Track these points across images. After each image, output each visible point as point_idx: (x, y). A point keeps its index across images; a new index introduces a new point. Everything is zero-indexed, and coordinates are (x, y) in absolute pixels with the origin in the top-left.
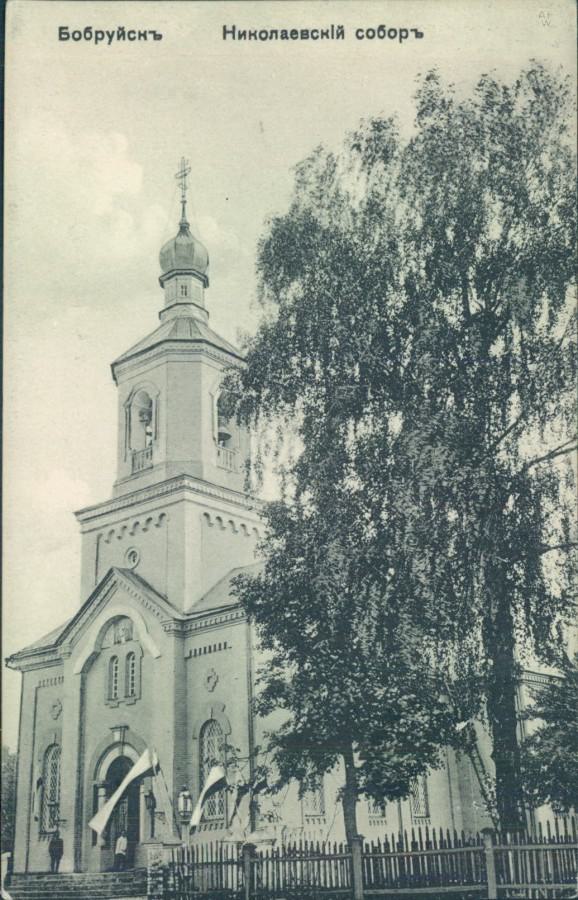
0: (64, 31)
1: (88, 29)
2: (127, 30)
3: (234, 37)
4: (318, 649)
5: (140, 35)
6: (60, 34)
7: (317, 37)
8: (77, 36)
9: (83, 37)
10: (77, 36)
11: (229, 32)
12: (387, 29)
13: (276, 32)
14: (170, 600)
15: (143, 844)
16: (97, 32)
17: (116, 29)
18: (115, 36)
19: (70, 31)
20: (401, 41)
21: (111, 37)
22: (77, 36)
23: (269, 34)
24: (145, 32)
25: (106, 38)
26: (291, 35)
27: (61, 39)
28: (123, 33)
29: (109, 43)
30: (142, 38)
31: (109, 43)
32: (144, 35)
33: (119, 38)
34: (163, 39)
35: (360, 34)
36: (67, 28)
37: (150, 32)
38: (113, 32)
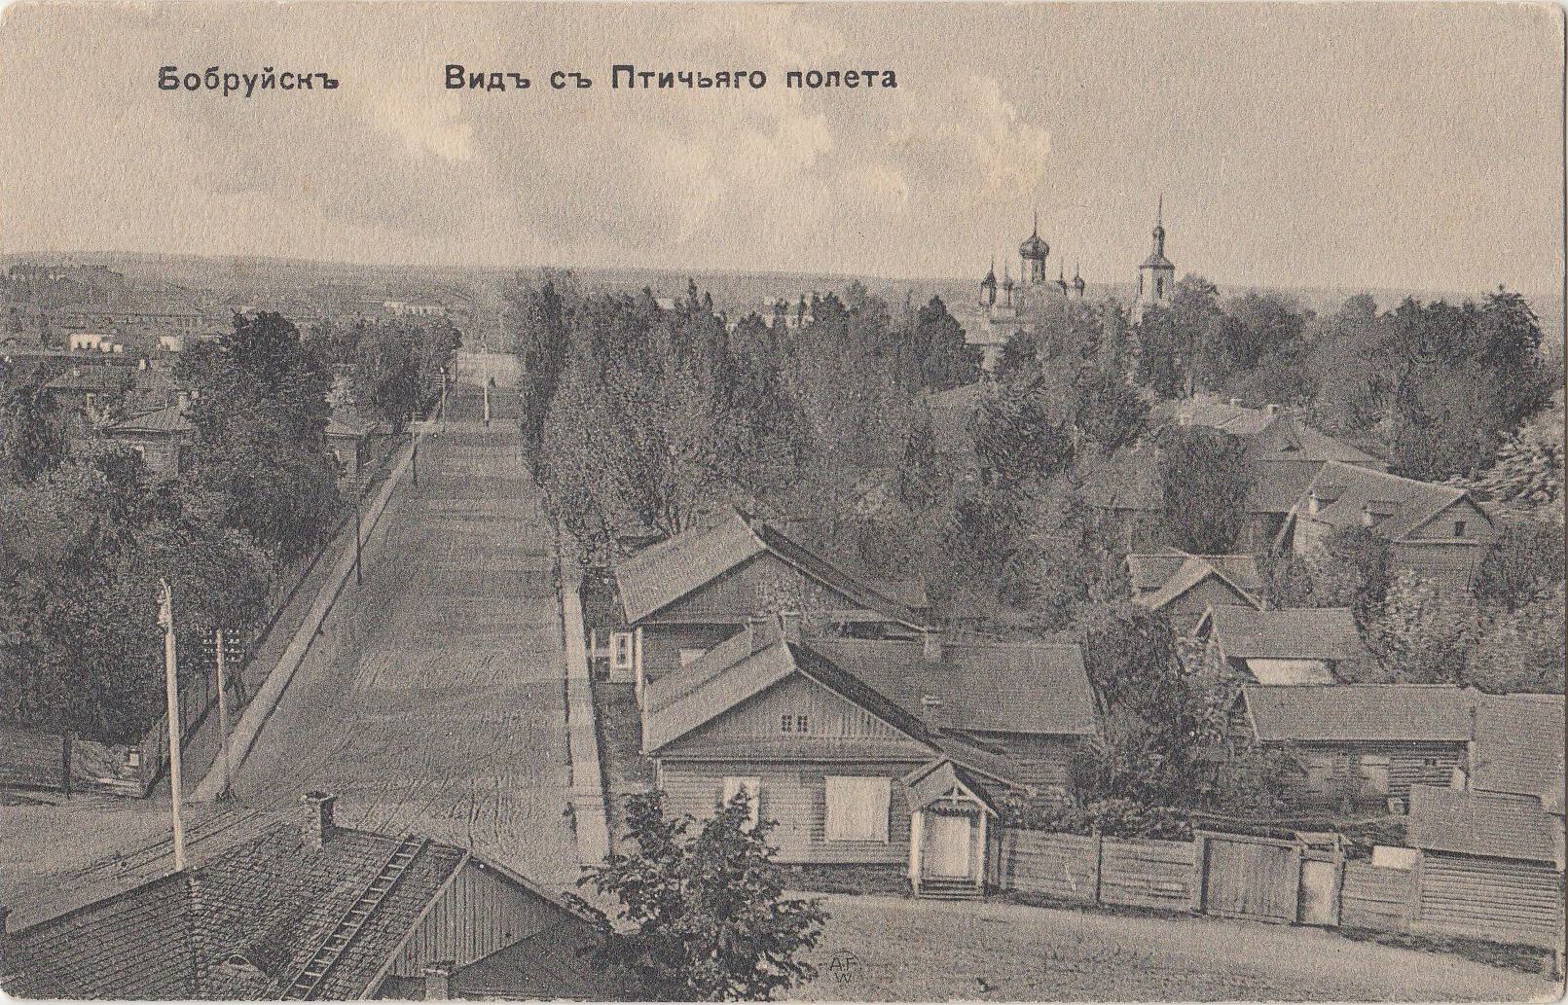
0: (168, 74)
1: (211, 72)
2: (278, 73)
3: (728, 86)
4: (214, 637)
5: (301, 80)
6: (163, 78)
7: (292, 86)
8: (192, 82)
9: (203, 84)
10: (193, 83)
11: (303, 81)
12: (220, 74)
13: (837, 75)
14: (1322, 931)
15: (67, 744)
16: (226, 77)
17: (260, 72)
18: (259, 82)
19: (180, 74)
20: (226, 94)
21: (251, 86)
22: (814, 79)
23: (825, 80)
24: (310, 76)
25: (243, 87)
26: (846, 78)
27: (449, 85)
28: (272, 78)
29: (248, 95)
30: (304, 85)
31: (248, 95)
32: (308, 81)
33: (264, 86)
34: (340, 83)
35: (559, 80)
36: (175, 69)
37: (318, 75)
38: (256, 76)
